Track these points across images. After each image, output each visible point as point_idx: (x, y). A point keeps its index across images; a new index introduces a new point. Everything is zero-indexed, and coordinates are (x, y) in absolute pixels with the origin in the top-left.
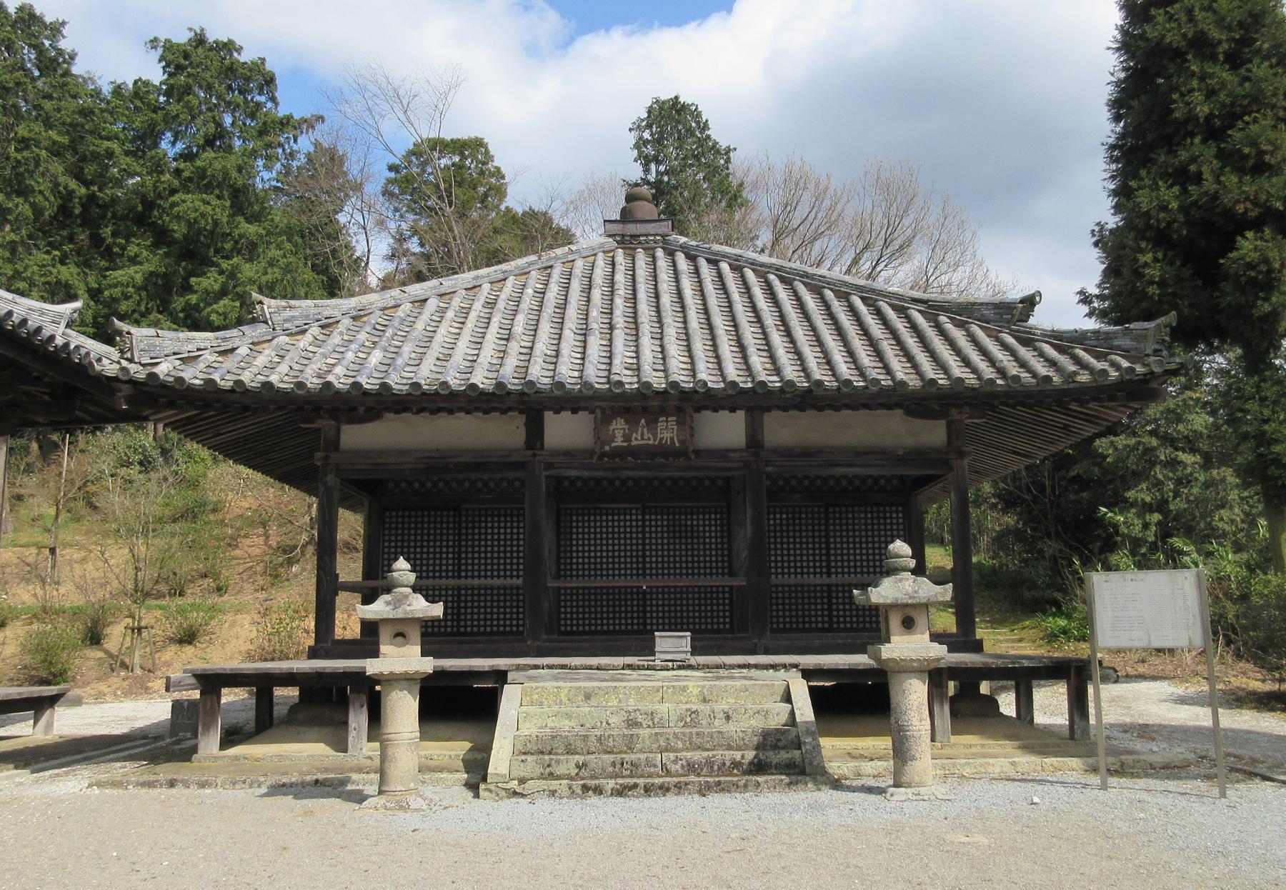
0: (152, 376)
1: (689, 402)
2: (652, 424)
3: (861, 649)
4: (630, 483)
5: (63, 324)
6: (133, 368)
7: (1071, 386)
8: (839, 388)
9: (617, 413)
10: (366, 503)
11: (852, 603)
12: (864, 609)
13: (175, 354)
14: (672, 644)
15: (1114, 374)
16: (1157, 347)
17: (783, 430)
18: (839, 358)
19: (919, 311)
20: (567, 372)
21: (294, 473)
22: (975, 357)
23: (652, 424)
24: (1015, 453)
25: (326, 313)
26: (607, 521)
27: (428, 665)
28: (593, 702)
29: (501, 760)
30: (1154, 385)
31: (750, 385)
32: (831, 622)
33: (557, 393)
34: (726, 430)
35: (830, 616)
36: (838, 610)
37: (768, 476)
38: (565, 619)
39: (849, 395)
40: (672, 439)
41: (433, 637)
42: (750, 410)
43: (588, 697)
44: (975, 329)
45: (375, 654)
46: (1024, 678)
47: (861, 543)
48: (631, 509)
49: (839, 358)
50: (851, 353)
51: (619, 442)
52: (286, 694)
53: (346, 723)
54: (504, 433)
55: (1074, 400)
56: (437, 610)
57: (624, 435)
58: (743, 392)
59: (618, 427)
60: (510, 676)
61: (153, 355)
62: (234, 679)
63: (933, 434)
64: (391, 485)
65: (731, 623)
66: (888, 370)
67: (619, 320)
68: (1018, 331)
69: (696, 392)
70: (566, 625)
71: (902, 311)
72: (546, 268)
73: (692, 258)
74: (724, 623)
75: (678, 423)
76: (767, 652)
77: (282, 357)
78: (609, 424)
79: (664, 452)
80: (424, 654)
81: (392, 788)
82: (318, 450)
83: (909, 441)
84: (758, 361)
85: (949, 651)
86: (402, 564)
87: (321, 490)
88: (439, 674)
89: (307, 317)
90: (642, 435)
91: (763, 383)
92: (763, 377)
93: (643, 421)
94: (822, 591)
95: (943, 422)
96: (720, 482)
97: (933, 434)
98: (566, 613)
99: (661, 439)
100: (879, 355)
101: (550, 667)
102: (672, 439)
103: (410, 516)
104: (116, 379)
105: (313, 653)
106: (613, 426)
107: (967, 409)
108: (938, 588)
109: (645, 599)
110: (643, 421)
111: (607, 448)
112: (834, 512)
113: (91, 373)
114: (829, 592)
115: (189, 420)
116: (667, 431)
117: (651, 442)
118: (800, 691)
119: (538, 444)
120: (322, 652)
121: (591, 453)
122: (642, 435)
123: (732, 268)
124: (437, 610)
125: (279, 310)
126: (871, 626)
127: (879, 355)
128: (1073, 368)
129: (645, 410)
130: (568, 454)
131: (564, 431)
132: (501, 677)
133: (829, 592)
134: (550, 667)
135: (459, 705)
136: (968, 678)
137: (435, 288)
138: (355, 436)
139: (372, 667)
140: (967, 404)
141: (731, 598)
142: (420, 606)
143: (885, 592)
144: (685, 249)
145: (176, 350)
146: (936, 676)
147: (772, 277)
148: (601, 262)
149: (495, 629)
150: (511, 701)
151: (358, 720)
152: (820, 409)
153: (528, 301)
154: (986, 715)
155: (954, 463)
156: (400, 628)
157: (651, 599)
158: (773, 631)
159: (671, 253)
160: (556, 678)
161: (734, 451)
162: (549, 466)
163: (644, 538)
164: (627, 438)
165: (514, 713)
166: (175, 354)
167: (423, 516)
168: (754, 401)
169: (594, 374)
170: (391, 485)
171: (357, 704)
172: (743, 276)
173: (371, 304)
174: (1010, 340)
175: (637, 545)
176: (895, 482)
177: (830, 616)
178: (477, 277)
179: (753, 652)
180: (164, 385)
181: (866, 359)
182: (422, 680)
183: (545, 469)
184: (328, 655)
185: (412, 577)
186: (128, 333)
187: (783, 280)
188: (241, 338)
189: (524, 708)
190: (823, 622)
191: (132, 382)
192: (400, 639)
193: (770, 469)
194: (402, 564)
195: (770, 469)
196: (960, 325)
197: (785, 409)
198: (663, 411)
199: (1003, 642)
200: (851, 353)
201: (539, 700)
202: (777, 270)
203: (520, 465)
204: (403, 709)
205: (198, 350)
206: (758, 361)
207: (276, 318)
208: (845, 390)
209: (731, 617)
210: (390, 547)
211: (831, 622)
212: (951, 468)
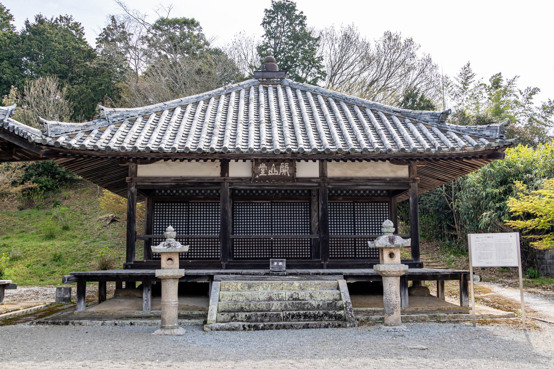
0: (57, 143)
1: (294, 158)
2: (277, 167)
3: (371, 267)
4: (243, 192)
5: (7, 116)
6: (48, 139)
7: (464, 151)
8: (362, 152)
9: (263, 161)
10: (146, 199)
11: (367, 246)
12: (373, 249)
13: (66, 133)
14: (279, 264)
15: (482, 148)
16: (501, 135)
17: (335, 170)
18: (361, 138)
19: (397, 116)
20: (240, 144)
21: (119, 187)
22: (421, 138)
23: (277, 167)
24: (438, 179)
25: (132, 114)
26: (250, 208)
27: (182, 272)
28: (252, 289)
29: (213, 315)
30: (499, 151)
31: (323, 150)
32: (355, 254)
33: (237, 153)
34: (308, 170)
35: (355, 252)
36: (359, 249)
37: (329, 189)
38: (236, 252)
39: (366, 155)
40: (286, 173)
41: (185, 261)
42: (322, 161)
43: (250, 287)
44: (421, 125)
45: (159, 267)
46: (441, 279)
47: (339, 216)
48: (266, 203)
49: (361, 138)
50: (366, 136)
51: (263, 174)
52: (111, 286)
53: (142, 297)
54: (211, 171)
55: (464, 158)
56: (186, 248)
57: (265, 171)
58: (319, 153)
59: (262, 167)
60: (215, 277)
61: (56, 133)
62: (92, 278)
63: (402, 172)
64: (157, 191)
65: (311, 255)
66: (382, 143)
67: (263, 119)
68: (441, 127)
69: (299, 153)
70: (236, 255)
71: (388, 116)
72: (228, 94)
73: (294, 90)
74: (308, 255)
75: (289, 166)
76: (328, 267)
77: (113, 135)
78: (259, 165)
79: (282, 178)
80: (181, 267)
81: (167, 326)
82: (128, 176)
83: (392, 175)
84: (325, 140)
85: (409, 268)
86: (170, 228)
87: (129, 194)
88: (187, 276)
89: (123, 116)
90: (273, 171)
91: (328, 149)
92: (328, 146)
93: (274, 165)
94: (351, 241)
95: (407, 166)
96: (306, 191)
97: (402, 172)
98: (236, 250)
99: (282, 173)
100: (379, 136)
101: (232, 274)
102: (286, 173)
103: (166, 206)
104: (41, 144)
105: (126, 267)
106: (260, 167)
107: (418, 161)
108: (405, 241)
109: (272, 244)
110: (274, 165)
111: (257, 177)
112: (357, 206)
113: (30, 141)
114: (355, 241)
115: (71, 162)
116: (285, 169)
117: (277, 174)
118: (343, 284)
119: (226, 175)
120: (130, 266)
121: (250, 179)
122: (273, 171)
123: (313, 95)
124: (186, 248)
125: (111, 113)
126: (374, 257)
127: (379, 136)
128: (464, 144)
129: (275, 160)
130: (241, 179)
131: (239, 170)
132: (211, 278)
133: (355, 241)
134: (232, 274)
135: (194, 289)
136: (418, 279)
137: (179, 102)
138: (145, 171)
139: (158, 273)
140: (418, 159)
141: (310, 244)
142: (180, 247)
143: (382, 241)
144: (290, 85)
145: (67, 131)
146: (404, 279)
147: (330, 99)
148: (253, 90)
149: (249, 256)
150: (215, 289)
151: (147, 295)
152: (353, 161)
153: (221, 108)
154: (424, 296)
155: (411, 184)
156: (170, 256)
157: (275, 244)
158: (330, 258)
159: (284, 88)
160: (235, 279)
161: (314, 178)
162: (231, 184)
163: (272, 216)
164: (266, 172)
165: (218, 293)
166: (66, 133)
167: (172, 206)
168: (324, 157)
169: (252, 144)
170: (157, 191)
171: (147, 289)
172: (306, 96)
173: (151, 110)
174: (438, 132)
175: (275, 222)
176: (385, 192)
177: (355, 252)
178: (197, 98)
179: (322, 267)
180: (62, 147)
181: (373, 139)
182: (180, 279)
183: (229, 186)
184: (133, 267)
185: (174, 234)
186: (46, 123)
187: (336, 101)
188: (95, 125)
189: (222, 292)
190: (352, 255)
191: (48, 145)
192: (170, 261)
193: (330, 186)
194: (170, 228)
195: (330, 186)
196: (415, 123)
197: (338, 161)
198: (284, 161)
199: (431, 263)
200: (366, 136)
201: (228, 291)
202: (321, 93)
203: (218, 184)
204: (170, 291)
205: (76, 131)
206: (325, 140)
207: (110, 117)
208: (364, 153)
209: (311, 252)
210: (157, 219)
211: (355, 254)
212: (410, 187)
